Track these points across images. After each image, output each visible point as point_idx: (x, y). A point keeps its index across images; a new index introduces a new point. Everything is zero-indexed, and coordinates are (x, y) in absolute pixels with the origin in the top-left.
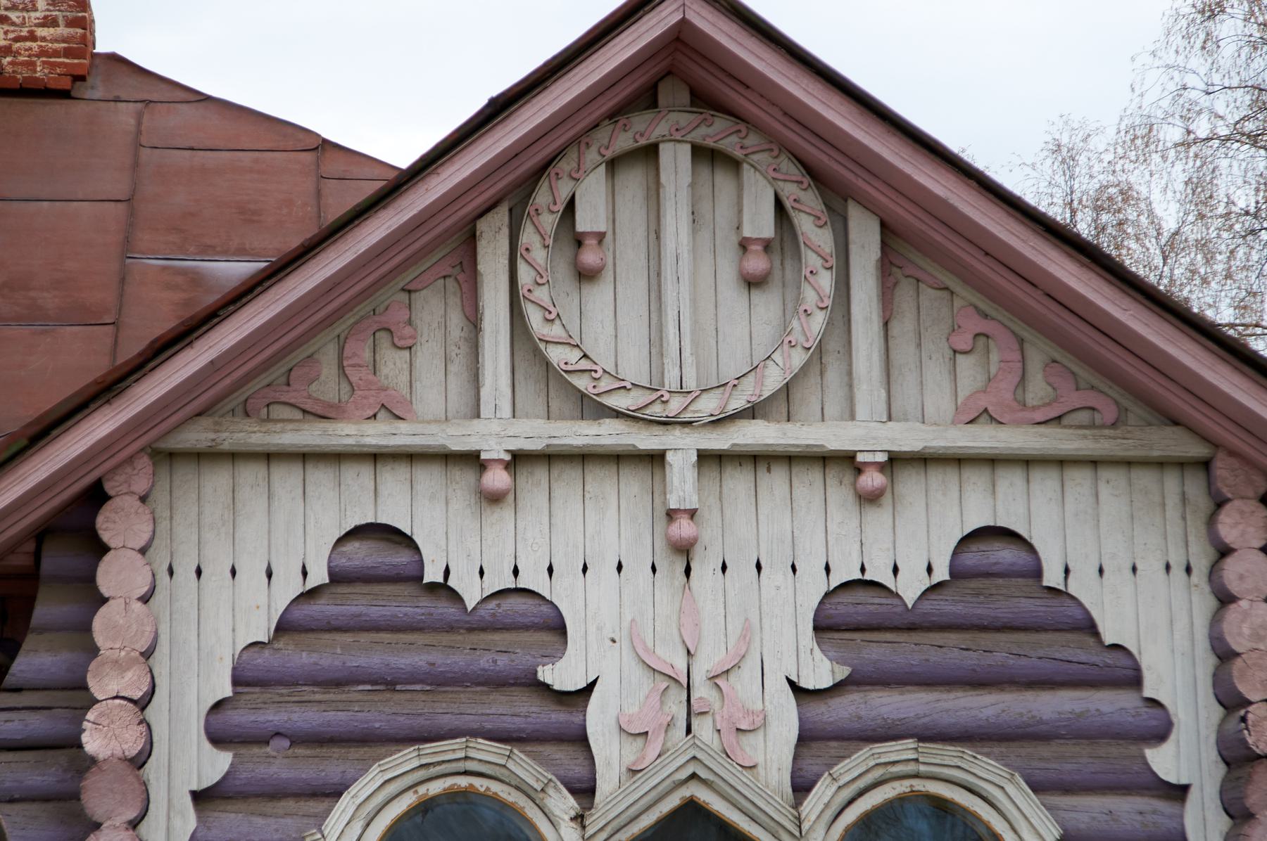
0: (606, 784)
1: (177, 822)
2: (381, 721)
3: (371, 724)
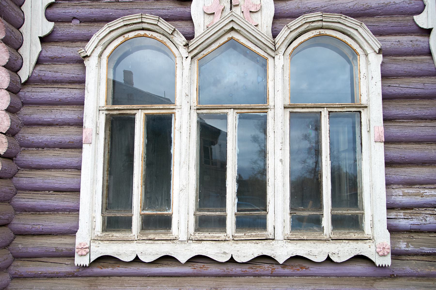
0: (199, 30)
1: (34, 48)
2: (112, 12)
3: (108, 13)
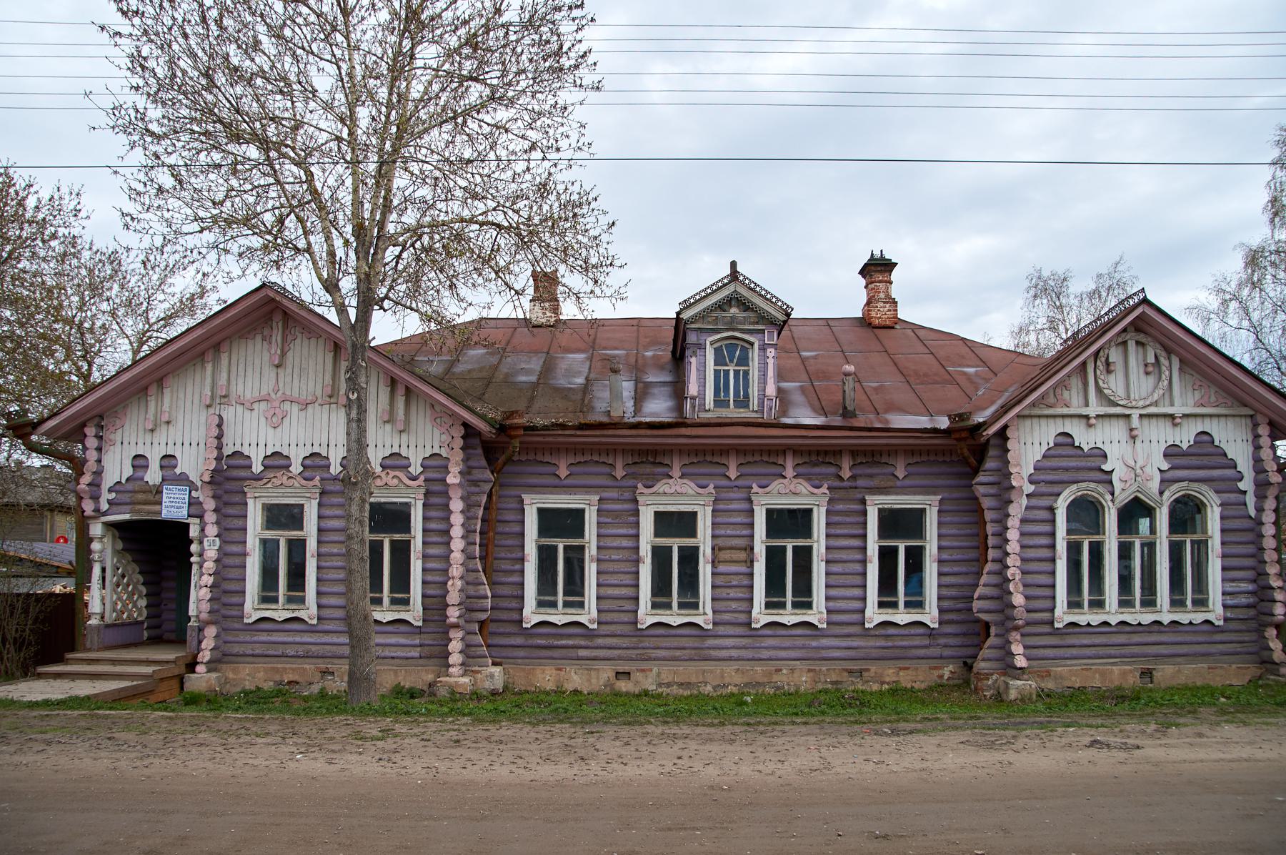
0: (1116, 493)
